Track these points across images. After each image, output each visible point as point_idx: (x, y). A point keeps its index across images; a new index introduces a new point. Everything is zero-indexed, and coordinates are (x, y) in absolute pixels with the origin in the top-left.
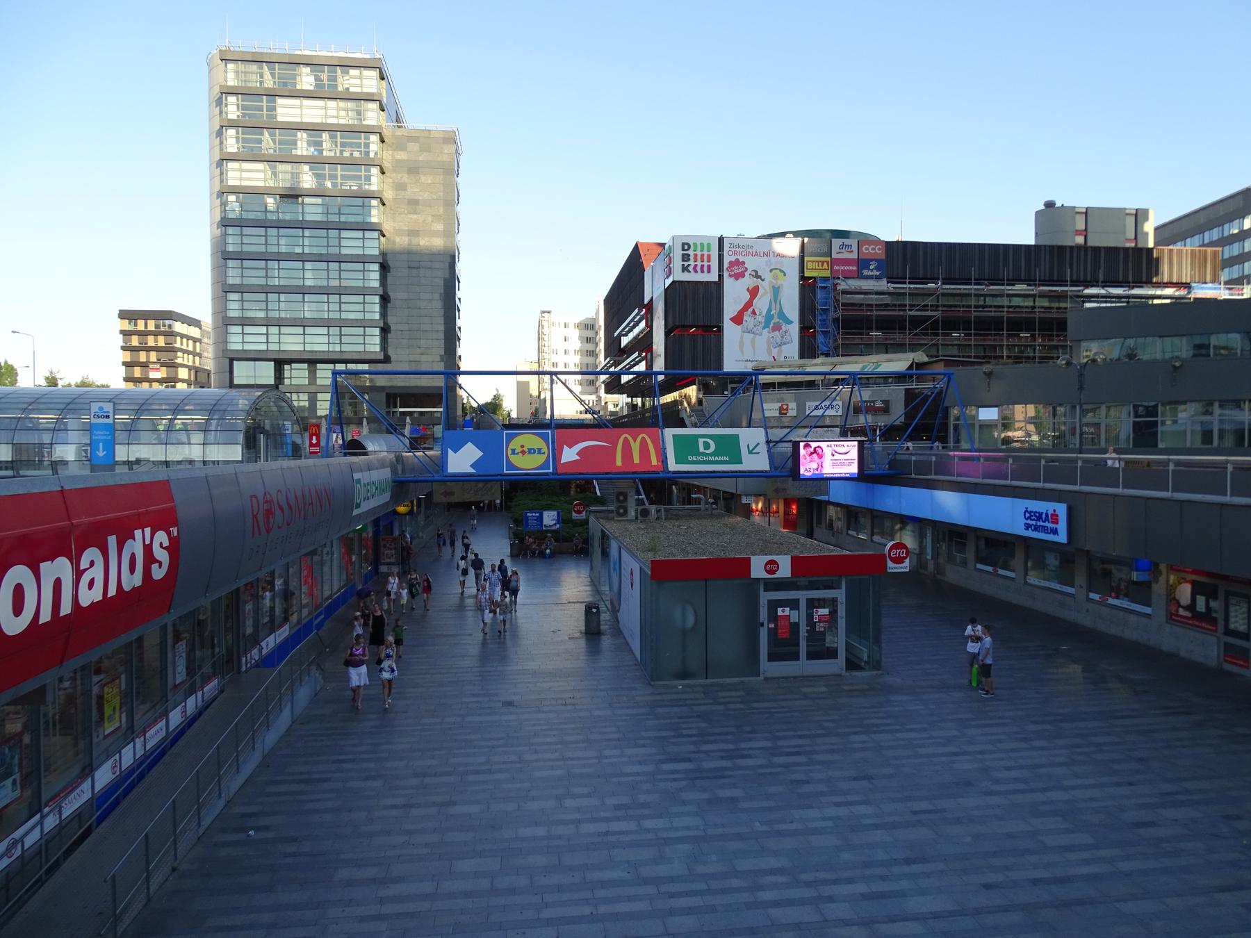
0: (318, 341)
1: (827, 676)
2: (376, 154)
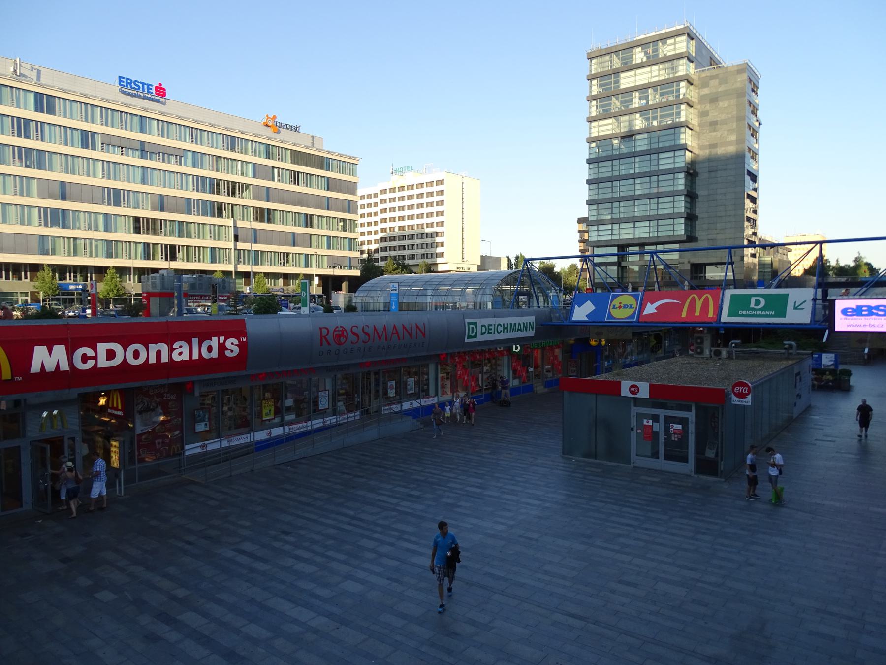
0: (644, 231)
1: (677, 474)
2: (684, 95)
